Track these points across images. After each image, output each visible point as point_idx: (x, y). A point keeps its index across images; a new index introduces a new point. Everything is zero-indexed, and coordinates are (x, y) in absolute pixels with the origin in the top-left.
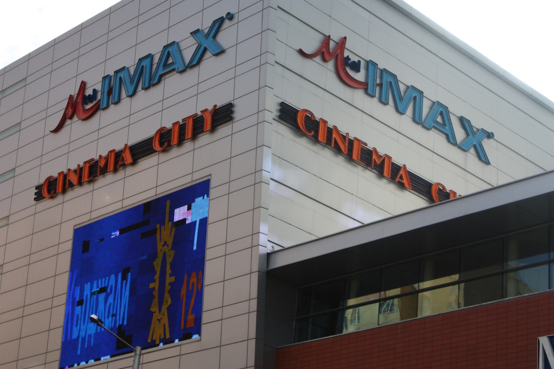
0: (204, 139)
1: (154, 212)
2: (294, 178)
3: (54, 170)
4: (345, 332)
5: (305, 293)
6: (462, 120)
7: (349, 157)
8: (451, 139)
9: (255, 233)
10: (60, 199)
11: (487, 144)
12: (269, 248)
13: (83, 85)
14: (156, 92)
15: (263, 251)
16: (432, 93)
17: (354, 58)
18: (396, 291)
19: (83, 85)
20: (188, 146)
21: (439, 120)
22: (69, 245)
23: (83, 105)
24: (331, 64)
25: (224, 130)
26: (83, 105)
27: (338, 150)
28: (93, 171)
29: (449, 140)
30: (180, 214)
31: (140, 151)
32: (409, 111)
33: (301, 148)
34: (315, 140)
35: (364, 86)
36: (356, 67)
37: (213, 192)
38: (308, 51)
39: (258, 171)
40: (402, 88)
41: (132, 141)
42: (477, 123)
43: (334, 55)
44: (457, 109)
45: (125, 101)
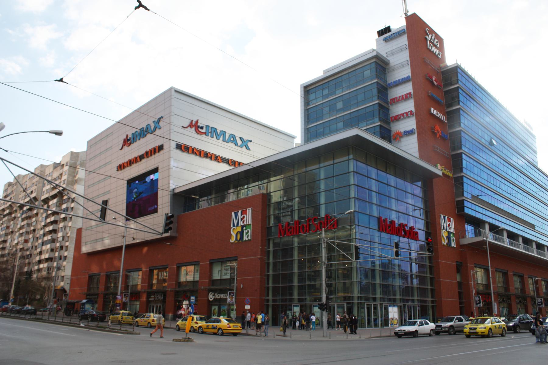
0: (157, 154)
1: (142, 178)
3: (121, 162)
5: (186, 199)
6: (240, 138)
7: (200, 155)
8: (236, 144)
9: (169, 183)
10: (123, 171)
11: (249, 144)
13: (127, 136)
14: (145, 139)
15: (171, 188)
16: (229, 132)
17: (201, 125)
18: (206, 198)
19: (127, 136)
20: (153, 156)
21: (233, 139)
23: (127, 142)
24: (193, 129)
25: (161, 152)
26: (127, 142)
27: (196, 154)
28: (130, 163)
30: (152, 177)
31: (141, 157)
35: (205, 133)
36: (202, 128)
37: (159, 171)
39: (169, 165)
40: (219, 132)
42: (245, 138)
43: (196, 126)
45: (138, 141)
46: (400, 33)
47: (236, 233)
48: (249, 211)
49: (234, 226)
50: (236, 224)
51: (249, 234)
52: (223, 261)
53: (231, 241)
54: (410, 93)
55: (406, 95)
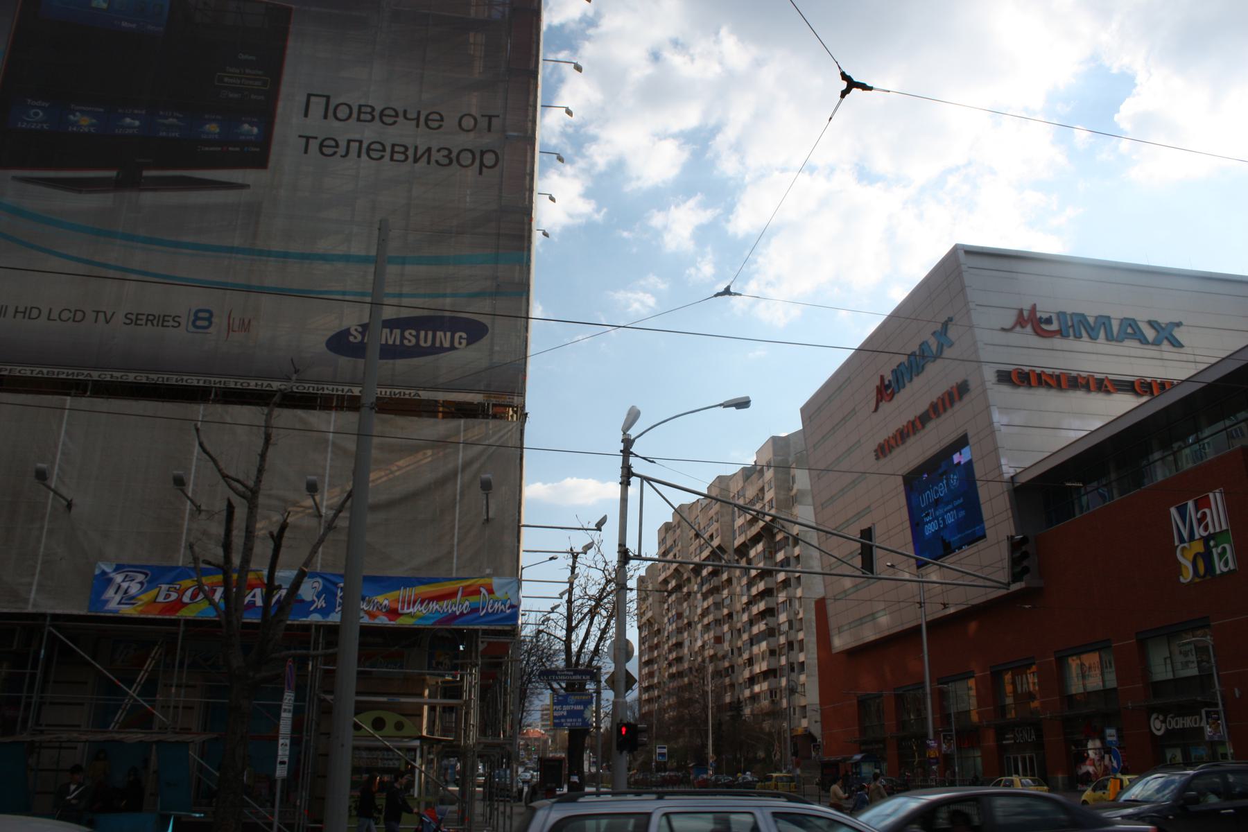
0: (957, 406)
2: (1018, 418)
6: (1151, 324)
8: (1143, 341)
11: (1179, 334)
12: (1012, 472)
13: (882, 378)
14: (922, 376)
15: (1007, 476)
17: (1045, 316)
19: (882, 378)
20: (950, 412)
21: (1131, 330)
22: (902, 487)
23: (885, 391)
25: (966, 398)
26: (885, 391)
27: (1049, 386)
28: (902, 436)
29: (1141, 342)
30: (956, 458)
33: (1021, 395)
34: (1030, 385)
38: (1007, 327)
39: (991, 423)
40: (1091, 320)
41: (918, 413)
42: (1163, 319)
44: (1141, 316)
45: (908, 385)
47: (1191, 558)
49: (1182, 540)
50: (1185, 535)
51: (1229, 554)
52: (1171, 633)
53: (1182, 580)
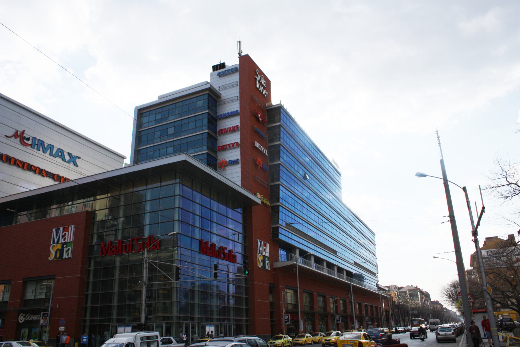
4: (48, 217)
8: (64, 160)
11: (78, 161)
17: (27, 137)
24: (18, 139)
27: (18, 166)
32: (48, 152)
35: (31, 145)
36: (28, 139)
38: (9, 135)
40: (46, 145)
42: (74, 154)
44: (66, 150)
46: (233, 71)
48: (72, 229)
49: (54, 243)
50: (56, 241)
51: (70, 251)
53: (49, 259)
54: (237, 126)
55: (234, 127)
